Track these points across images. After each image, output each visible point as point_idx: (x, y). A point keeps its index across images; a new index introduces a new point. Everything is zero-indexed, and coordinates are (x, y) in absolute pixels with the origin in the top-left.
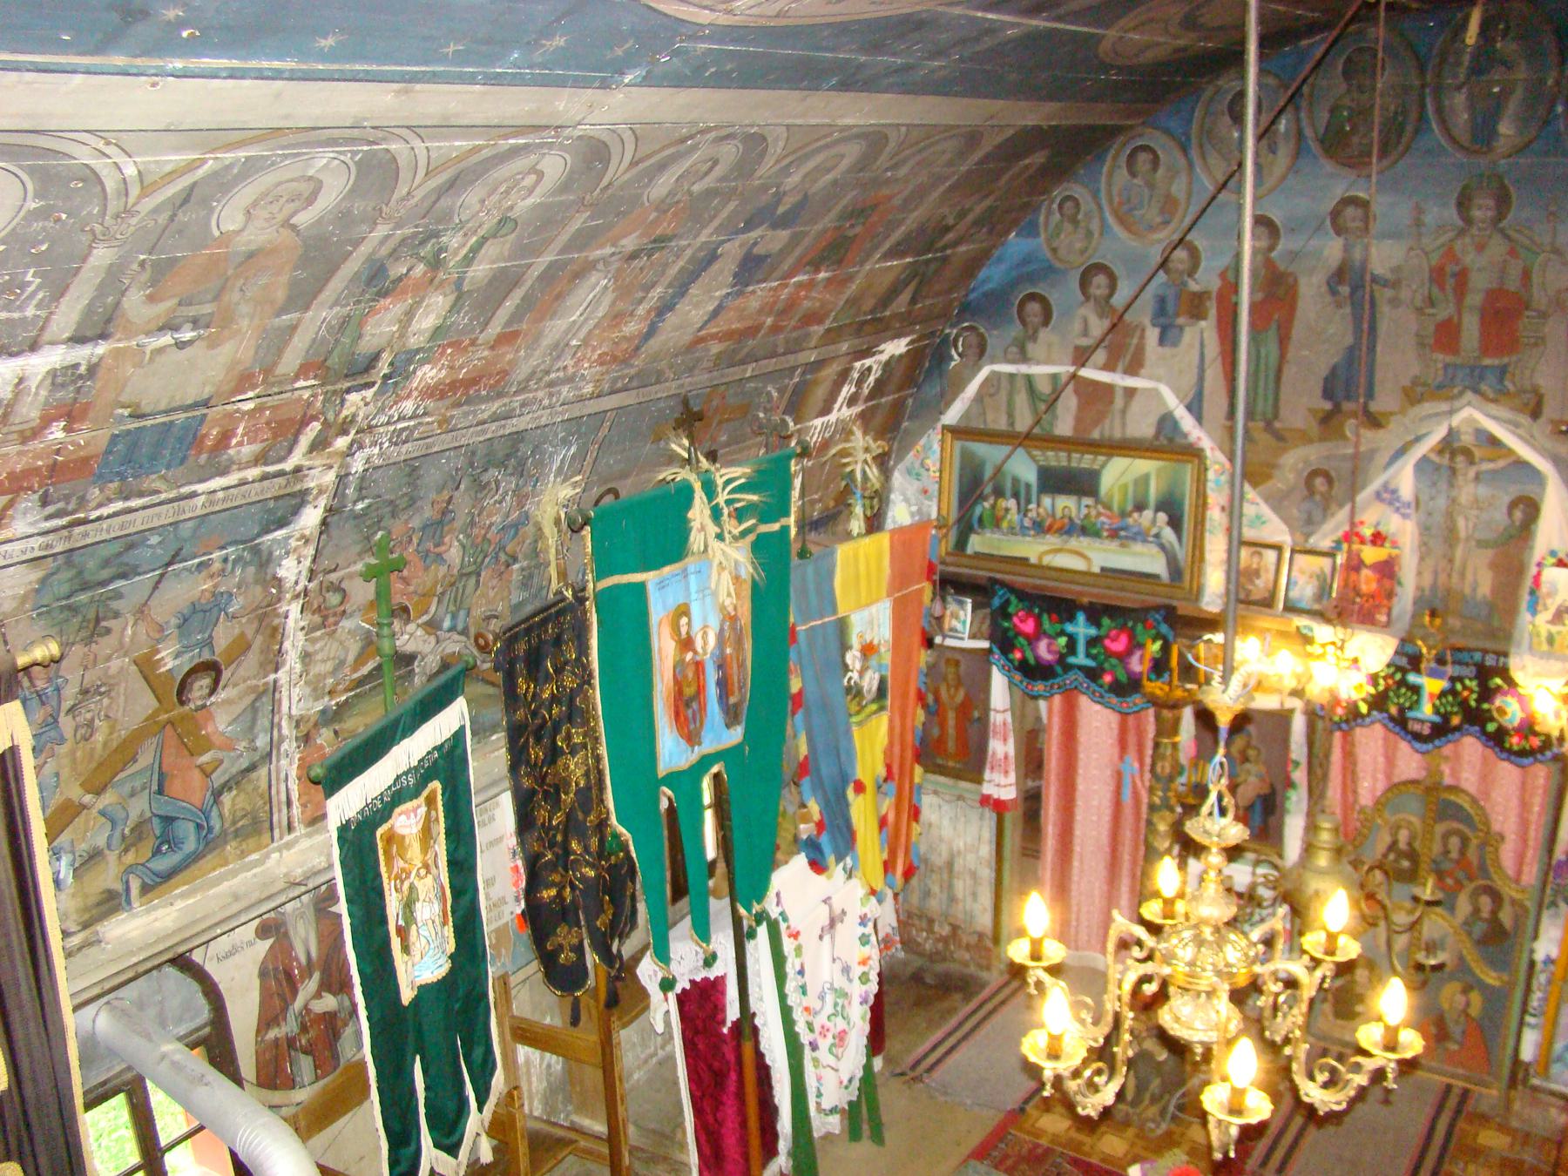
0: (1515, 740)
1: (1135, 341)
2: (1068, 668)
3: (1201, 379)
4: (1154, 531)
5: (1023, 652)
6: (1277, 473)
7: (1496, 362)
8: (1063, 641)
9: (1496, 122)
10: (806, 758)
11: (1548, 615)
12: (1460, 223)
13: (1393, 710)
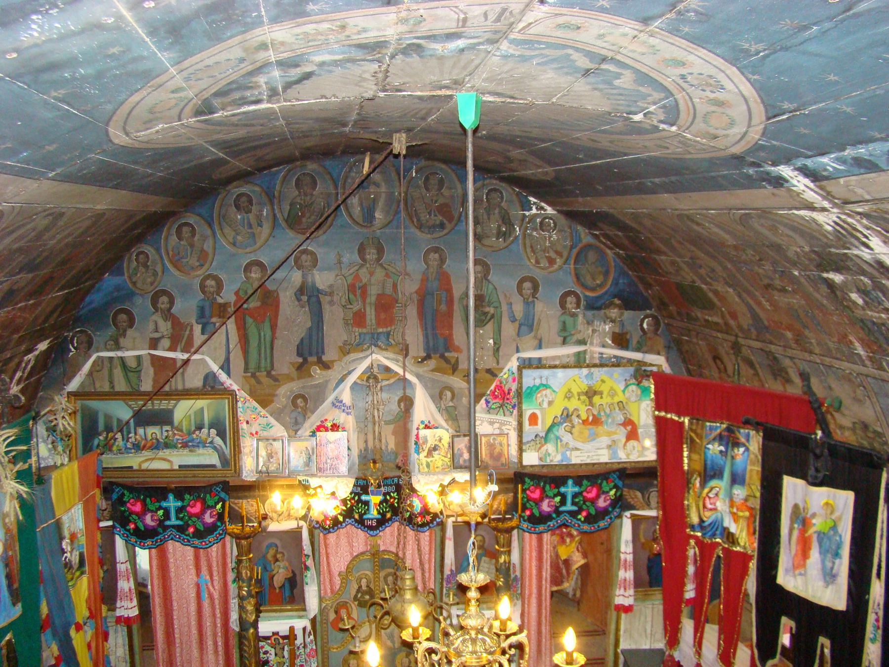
0: (419, 519)
1: (187, 333)
2: (166, 528)
3: (228, 352)
4: (209, 440)
5: (135, 524)
6: (275, 398)
7: (385, 330)
8: (161, 512)
9: (374, 212)
10: (48, 615)
11: (425, 453)
12: (361, 262)
13: (357, 516)
